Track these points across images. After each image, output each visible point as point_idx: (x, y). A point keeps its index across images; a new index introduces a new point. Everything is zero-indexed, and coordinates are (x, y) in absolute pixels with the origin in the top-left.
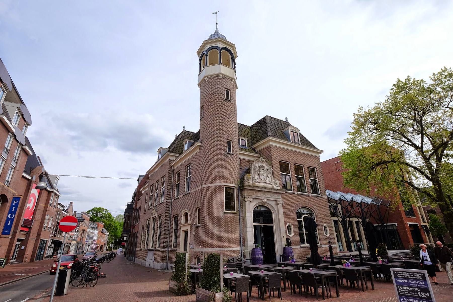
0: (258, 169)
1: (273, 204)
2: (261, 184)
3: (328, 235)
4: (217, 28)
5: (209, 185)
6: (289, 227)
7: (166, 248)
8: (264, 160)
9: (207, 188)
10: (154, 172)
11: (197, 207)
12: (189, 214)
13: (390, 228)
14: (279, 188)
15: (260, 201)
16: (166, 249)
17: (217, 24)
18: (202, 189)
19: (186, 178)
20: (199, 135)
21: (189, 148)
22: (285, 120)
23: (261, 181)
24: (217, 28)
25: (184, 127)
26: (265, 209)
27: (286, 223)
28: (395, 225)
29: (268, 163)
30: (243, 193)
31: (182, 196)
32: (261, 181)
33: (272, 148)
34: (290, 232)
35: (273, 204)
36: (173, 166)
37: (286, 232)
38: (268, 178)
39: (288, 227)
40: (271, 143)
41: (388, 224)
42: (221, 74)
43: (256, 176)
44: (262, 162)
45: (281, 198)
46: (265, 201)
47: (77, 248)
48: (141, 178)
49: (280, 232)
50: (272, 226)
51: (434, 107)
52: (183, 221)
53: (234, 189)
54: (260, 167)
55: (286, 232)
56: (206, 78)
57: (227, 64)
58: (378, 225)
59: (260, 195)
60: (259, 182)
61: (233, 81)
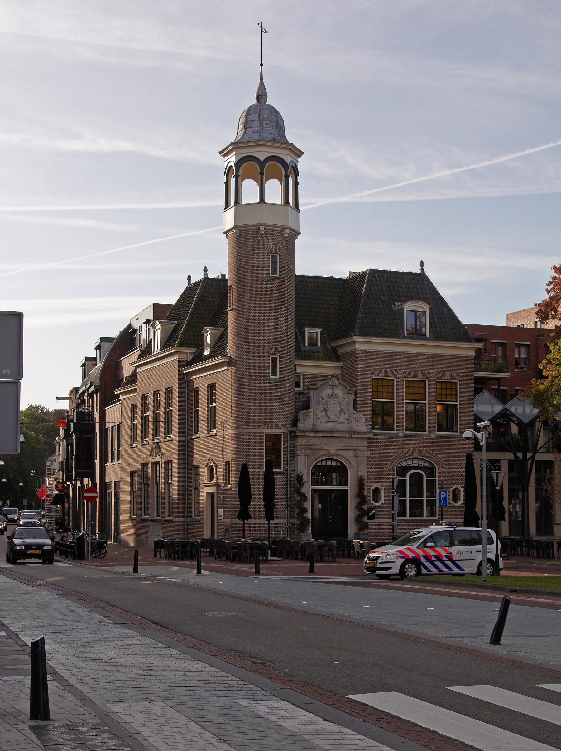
2: (330, 426)
4: (261, 79)
8: (337, 382)
14: (364, 429)
17: (262, 65)
22: (417, 270)
24: (261, 79)
26: (334, 464)
29: (346, 387)
35: (350, 455)
38: (342, 414)
42: (261, 225)
44: (333, 385)
46: (332, 452)
48: (107, 347)
50: (347, 490)
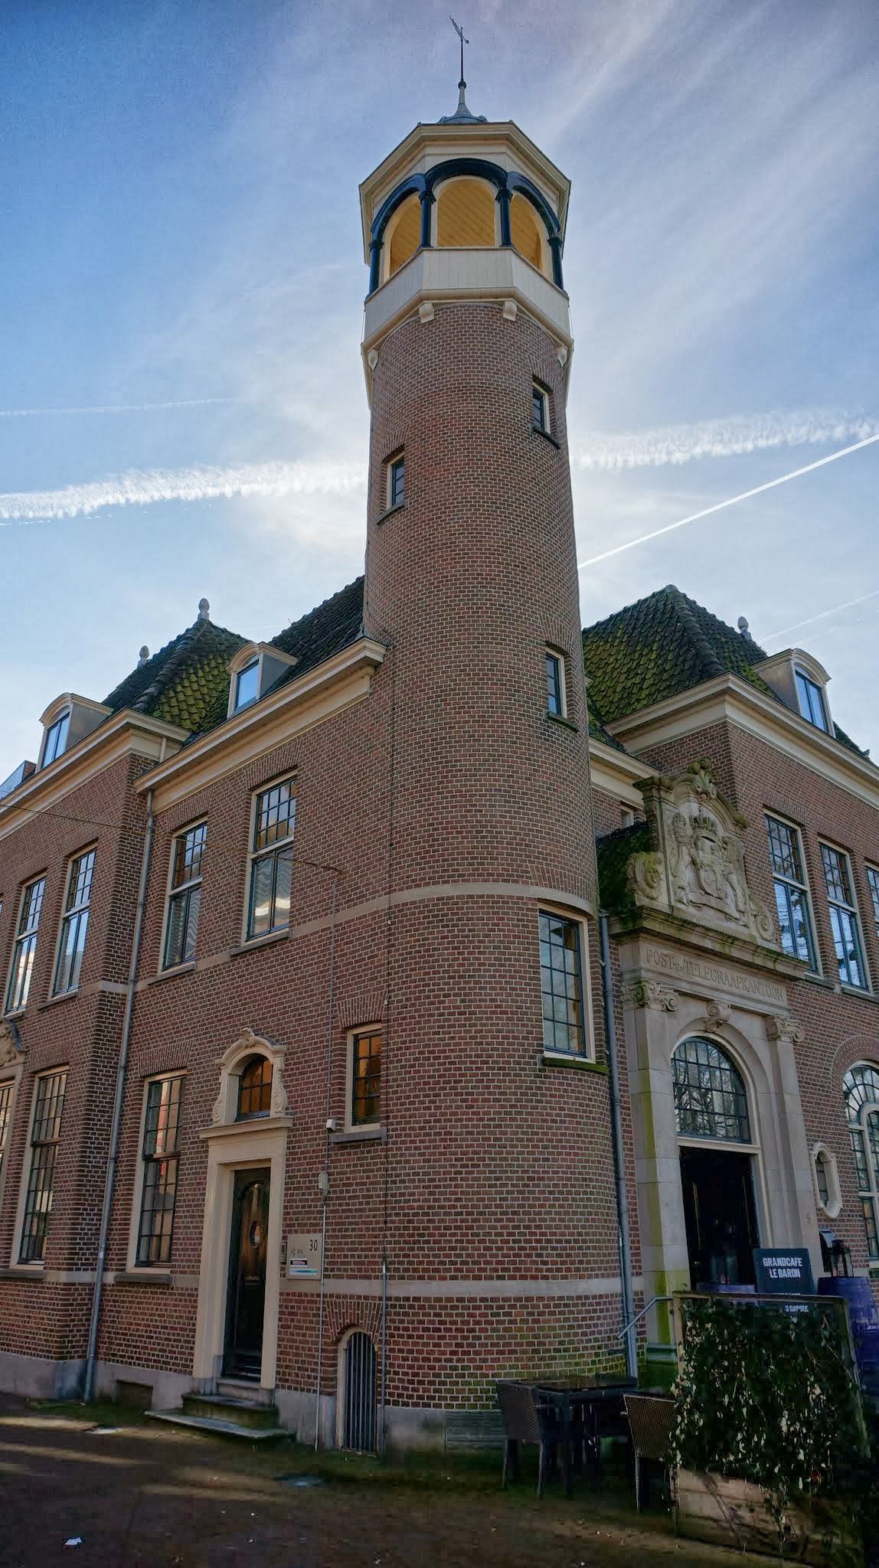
7: (90, 1266)
9: (440, 912)
10: (42, 806)
11: (344, 1022)
12: (277, 1062)
16: (85, 1277)
18: (395, 912)
19: (169, 892)
20: (359, 607)
21: (270, 689)
23: (705, 899)
25: (204, 605)
31: (223, 957)
32: (705, 899)
35: (752, 1028)
36: (152, 790)
40: (733, 713)
42: (511, 296)
43: (682, 867)
45: (784, 1003)
46: (724, 1012)
47: (369, 1065)
50: (745, 1160)
52: (224, 1107)
56: (427, 306)
57: (534, 261)
59: (705, 976)
61: (564, 351)
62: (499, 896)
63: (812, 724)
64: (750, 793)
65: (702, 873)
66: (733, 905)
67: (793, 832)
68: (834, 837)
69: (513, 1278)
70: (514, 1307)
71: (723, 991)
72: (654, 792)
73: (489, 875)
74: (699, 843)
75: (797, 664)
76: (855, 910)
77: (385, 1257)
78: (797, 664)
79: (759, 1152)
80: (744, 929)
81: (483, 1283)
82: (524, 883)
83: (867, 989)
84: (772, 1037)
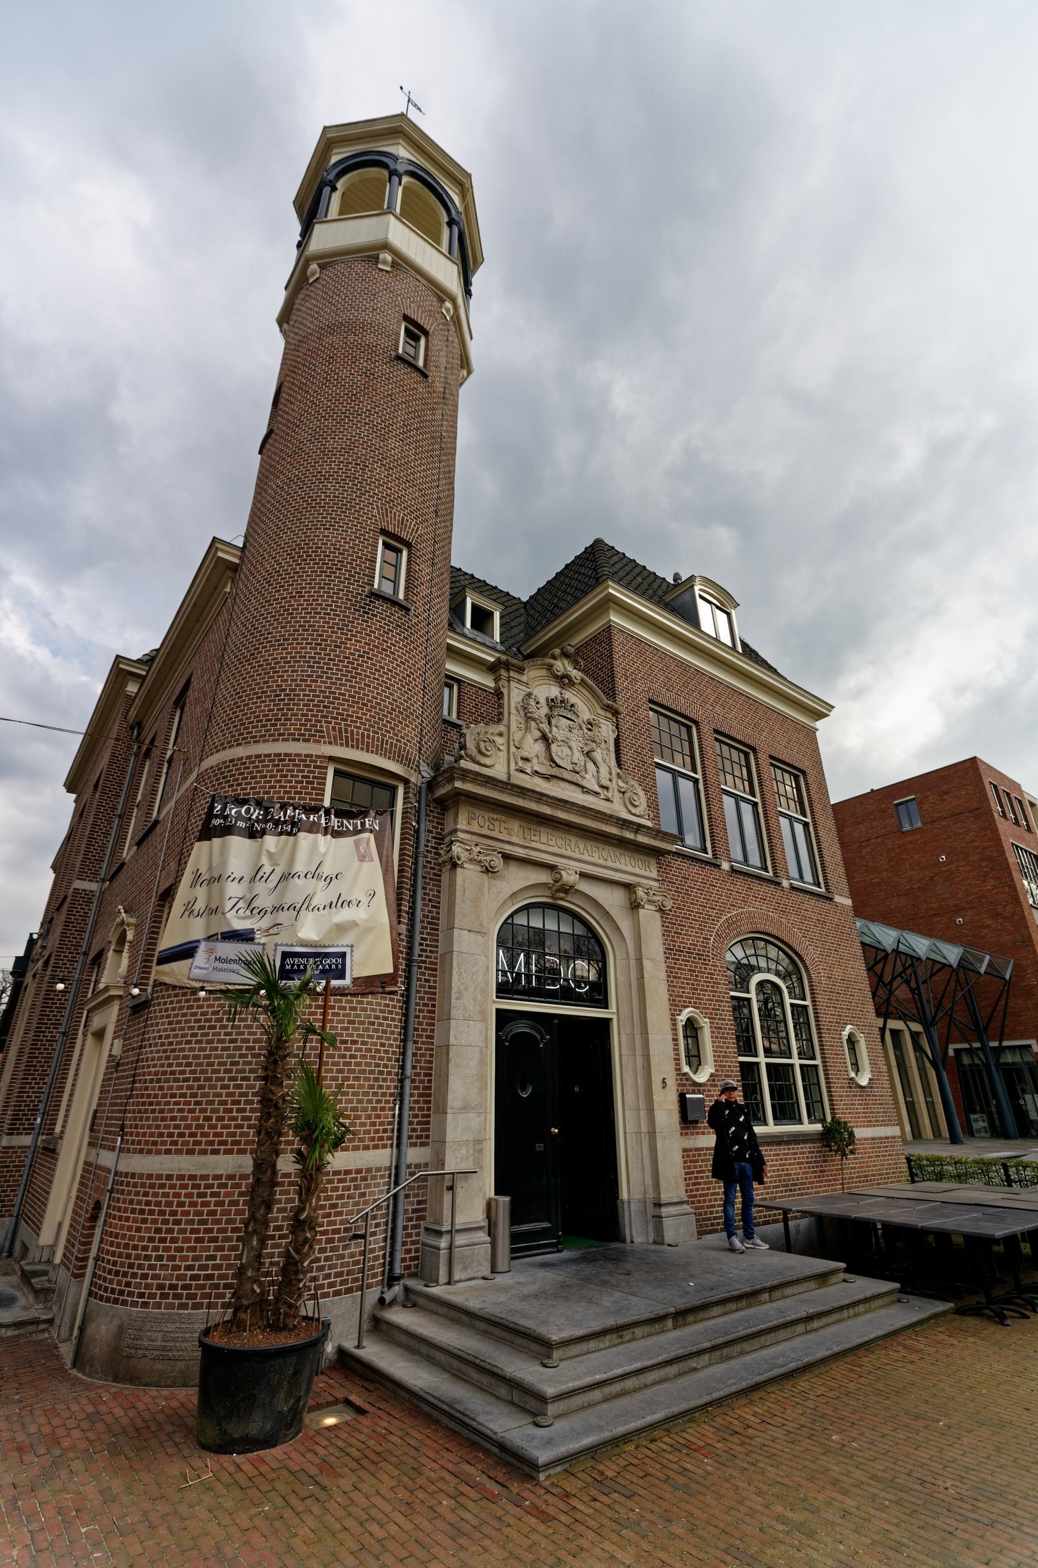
0: (544, 711)
1: (611, 899)
3: (864, 1081)
5: (241, 752)
6: (692, 1028)
13: (1008, 1058)
15: (543, 877)
27: (676, 1007)
28: (1030, 1046)
30: (449, 818)
32: (555, 771)
33: (617, 639)
34: (695, 1059)
35: (611, 899)
37: (677, 1060)
38: (590, 766)
39: (685, 1027)
41: (1005, 1043)
43: (529, 740)
45: (654, 874)
46: (569, 877)
49: (647, 1056)
50: (607, 1022)
51: (384, 1436)
53: (394, 789)
54: (552, 704)
55: (677, 1060)
58: (966, 1046)
59: (547, 845)
60: (548, 778)
62: (286, 755)
63: (717, 640)
64: (633, 686)
65: (554, 747)
66: (594, 781)
67: (746, 755)
68: (734, 735)
69: (229, 1152)
70: (224, 1186)
71: (570, 858)
72: (503, 673)
73: (280, 735)
74: (553, 721)
75: (700, 590)
76: (808, 820)
77: (122, 1129)
78: (700, 590)
79: (615, 1018)
80: (607, 804)
81: (196, 1158)
82: (315, 741)
83: (766, 870)
84: (635, 906)
